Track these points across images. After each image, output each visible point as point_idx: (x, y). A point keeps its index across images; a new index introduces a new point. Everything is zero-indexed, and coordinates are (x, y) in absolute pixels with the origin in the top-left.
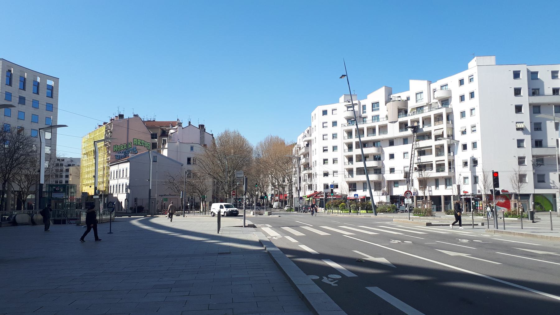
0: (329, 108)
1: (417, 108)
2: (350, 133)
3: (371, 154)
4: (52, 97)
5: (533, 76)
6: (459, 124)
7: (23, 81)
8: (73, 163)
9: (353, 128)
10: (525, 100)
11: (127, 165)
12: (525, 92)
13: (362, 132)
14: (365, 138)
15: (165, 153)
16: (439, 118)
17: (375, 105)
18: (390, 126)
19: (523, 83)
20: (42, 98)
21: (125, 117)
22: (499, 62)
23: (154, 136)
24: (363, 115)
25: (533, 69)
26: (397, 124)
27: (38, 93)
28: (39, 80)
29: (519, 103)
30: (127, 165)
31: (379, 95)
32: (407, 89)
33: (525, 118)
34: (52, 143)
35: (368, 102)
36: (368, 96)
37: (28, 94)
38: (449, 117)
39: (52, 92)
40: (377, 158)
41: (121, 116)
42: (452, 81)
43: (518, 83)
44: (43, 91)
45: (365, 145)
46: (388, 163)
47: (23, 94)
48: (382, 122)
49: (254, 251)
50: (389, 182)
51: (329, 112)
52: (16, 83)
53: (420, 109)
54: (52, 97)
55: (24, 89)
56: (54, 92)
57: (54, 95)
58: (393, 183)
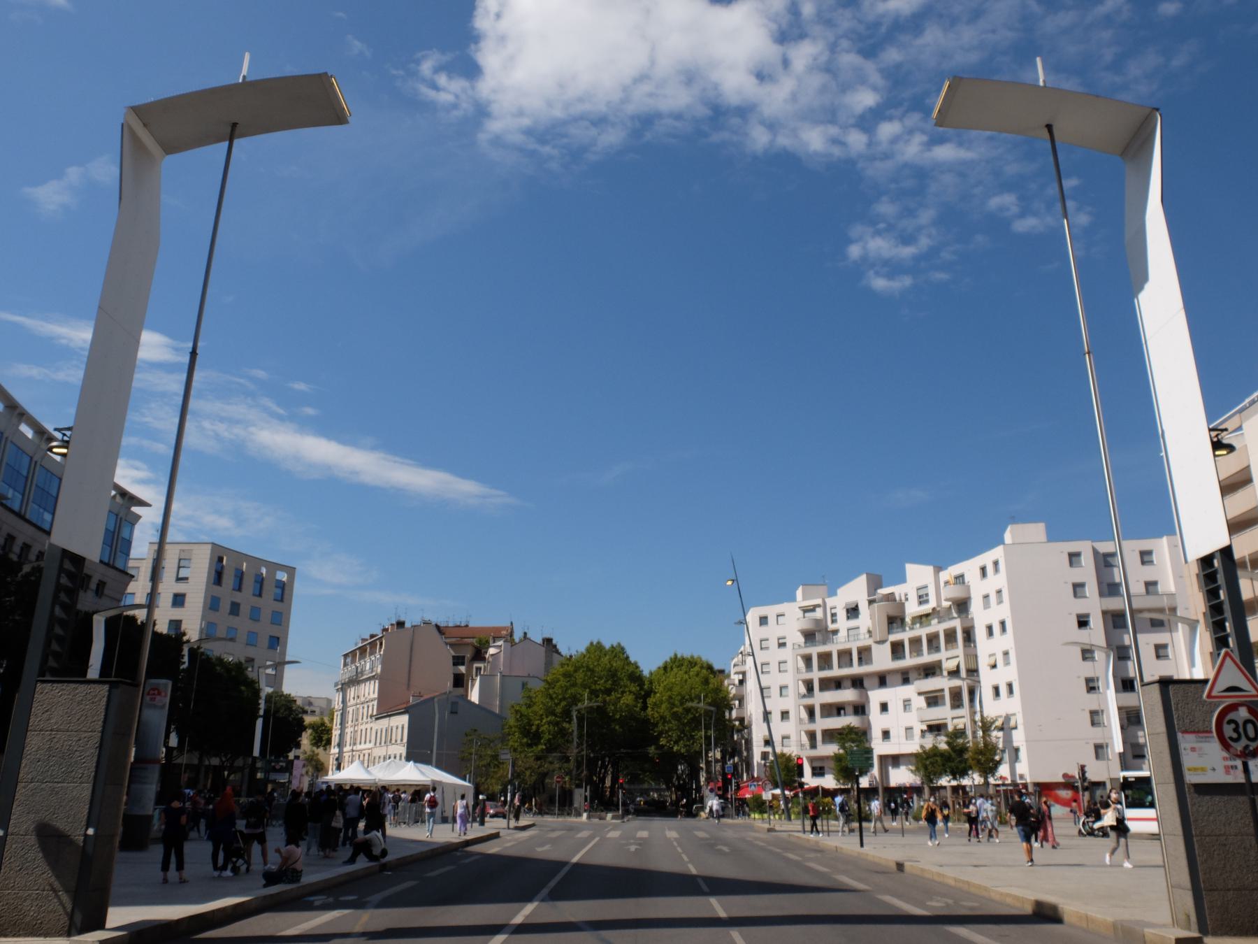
0: (770, 611)
1: (921, 617)
2: (808, 660)
3: (849, 703)
4: (282, 600)
5: (1104, 562)
6: (985, 647)
7: (240, 576)
8: (1006, 727)
9: (815, 651)
10: (1093, 604)
11: (404, 720)
12: (1092, 589)
13: (847, 658)
14: (836, 672)
15: (474, 696)
16: (950, 636)
17: (853, 612)
18: (876, 650)
19: (1087, 572)
20: (267, 603)
21: (408, 625)
22: (1052, 536)
23: (458, 661)
24: (831, 627)
25: (1105, 547)
26: (888, 646)
27: (260, 595)
28: (264, 571)
29: (1083, 611)
30: (404, 720)
31: (856, 590)
32: (902, 579)
33: (1096, 633)
34: (277, 680)
35: (839, 602)
36: (839, 591)
37: (246, 598)
38: (969, 636)
39: (283, 592)
40: (860, 709)
41: (400, 624)
42: (969, 568)
43: (1077, 575)
44: (270, 591)
45: (842, 682)
46: (877, 721)
47: (238, 597)
48: (865, 641)
49: (578, 852)
50: (883, 758)
51: (772, 620)
52: (229, 579)
53: (923, 619)
54: (282, 600)
55: (240, 589)
56: (286, 592)
57: (286, 596)
58: (890, 760)
